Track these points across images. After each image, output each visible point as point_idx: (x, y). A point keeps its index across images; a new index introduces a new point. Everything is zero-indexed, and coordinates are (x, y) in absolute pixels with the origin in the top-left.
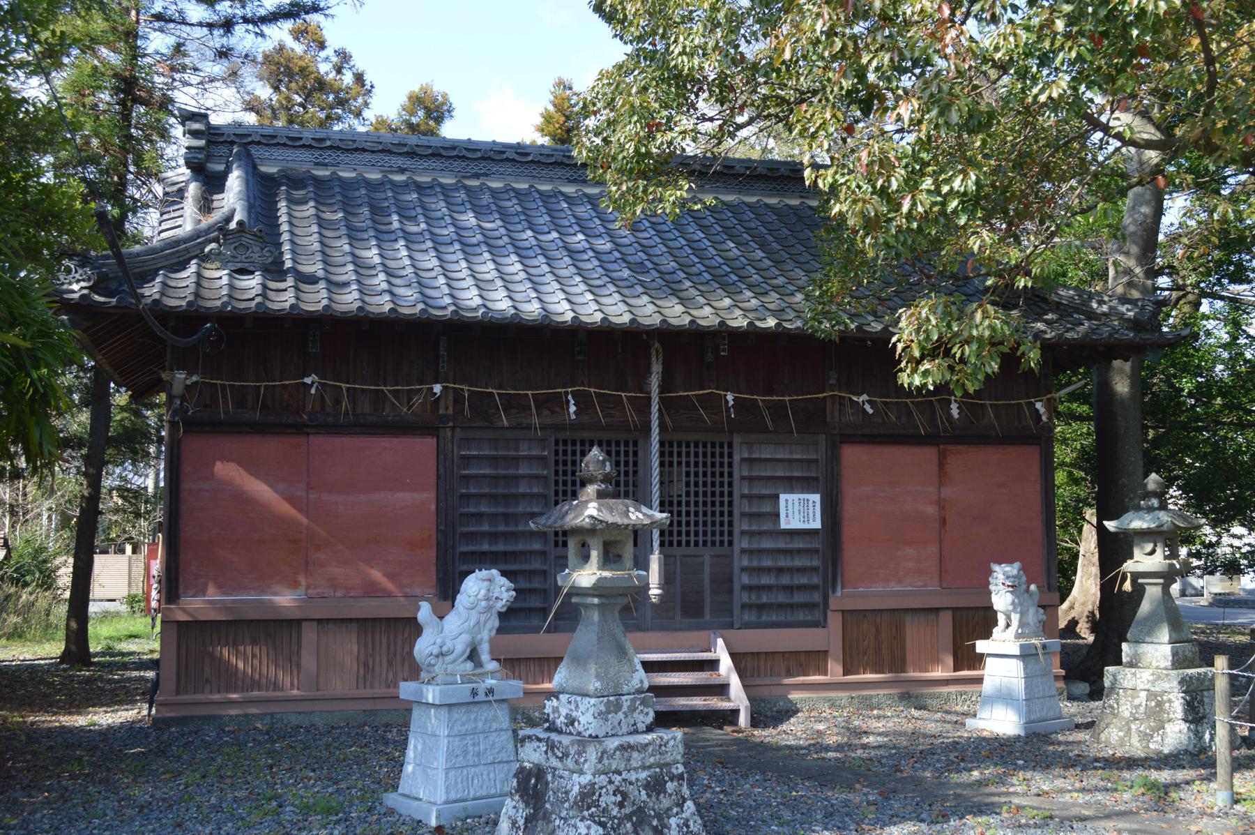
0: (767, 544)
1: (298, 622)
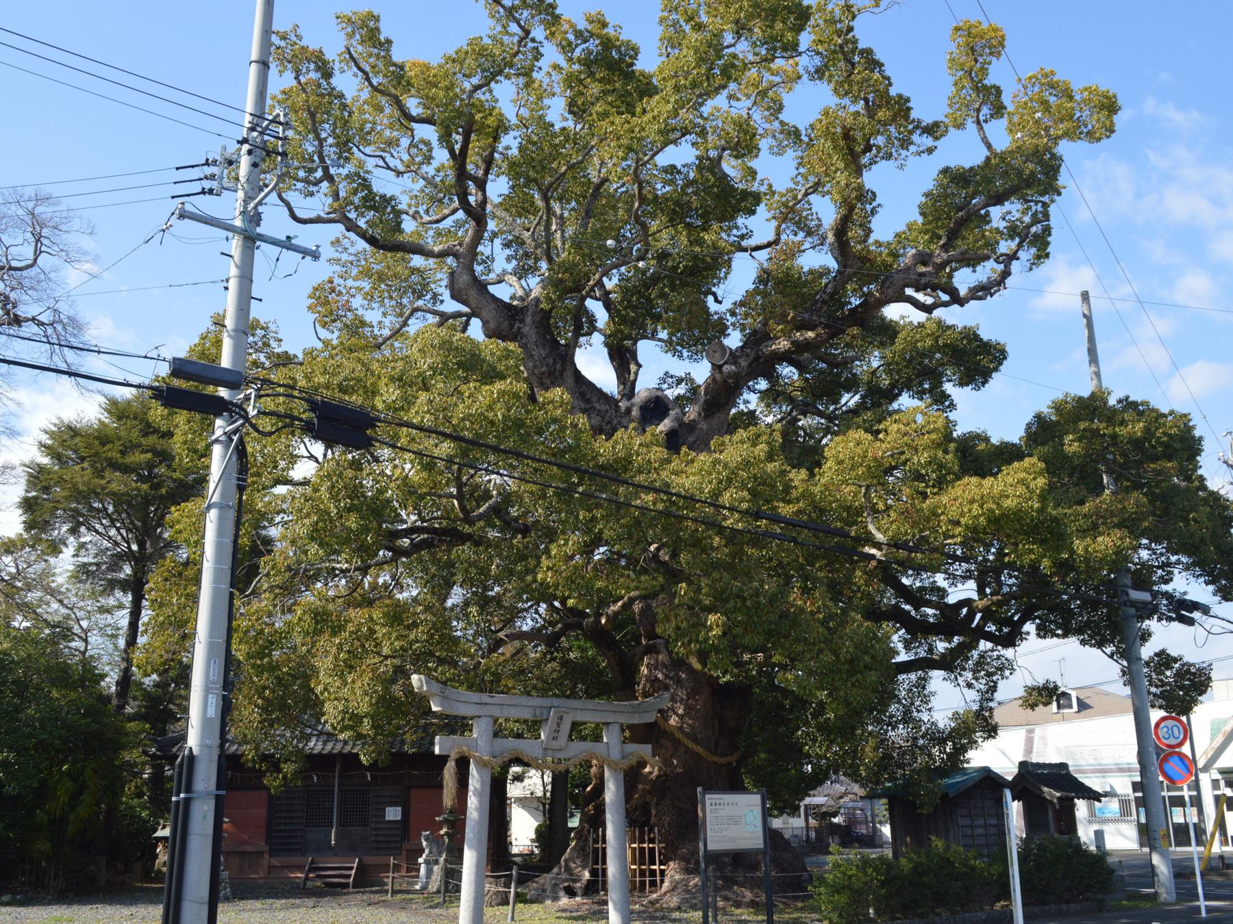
0: (382, 826)
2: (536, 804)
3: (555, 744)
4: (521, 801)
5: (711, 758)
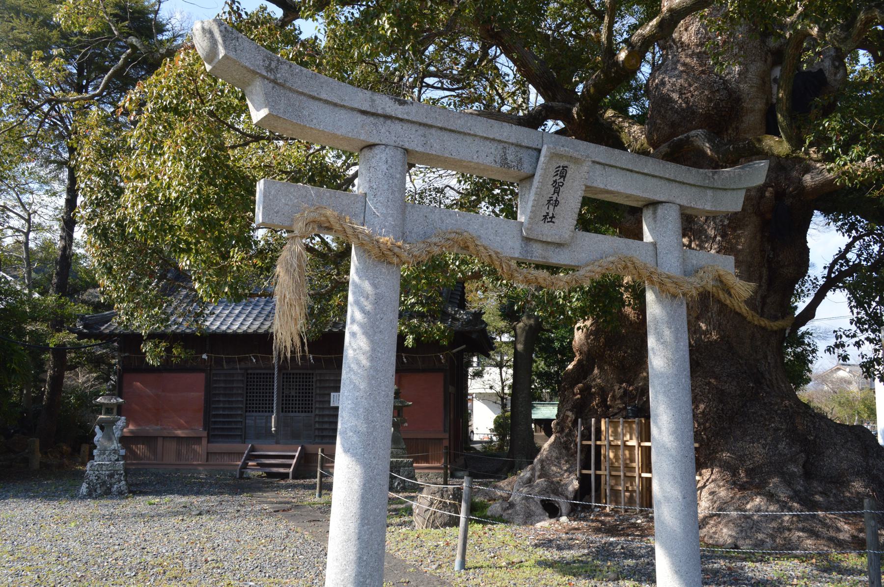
0: (327, 412)
1: (156, 438)
2: (494, 398)
3: (548, 232)
4: (482, 397)
5: (757, 320)
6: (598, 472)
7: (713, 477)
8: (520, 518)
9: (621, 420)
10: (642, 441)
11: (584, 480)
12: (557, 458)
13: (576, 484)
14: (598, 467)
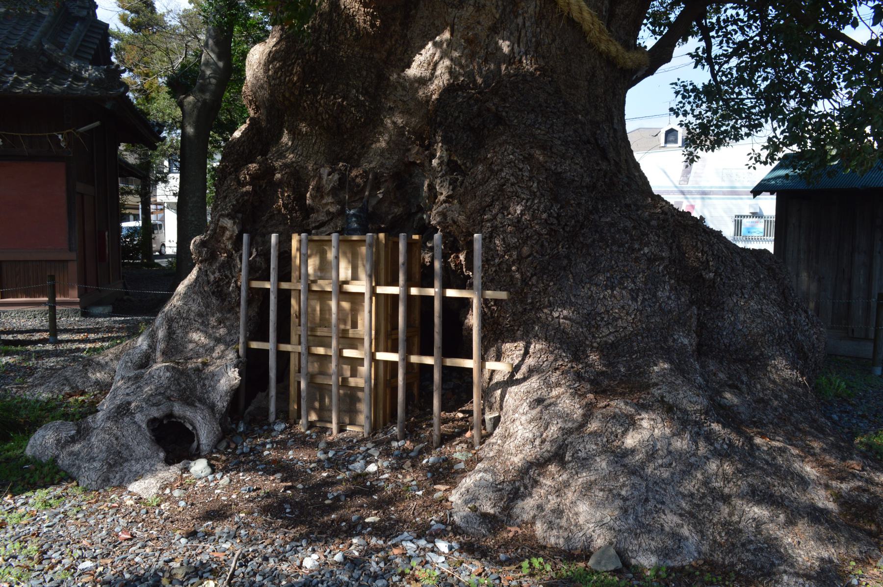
6: (284, 347)
7: (530, 361)
8: (89, 474)
9: (334, 237)
10: (378, 284)
11: (253, 366)
12: (200, 315)
13: (232, 377)
14: (284, 336)
